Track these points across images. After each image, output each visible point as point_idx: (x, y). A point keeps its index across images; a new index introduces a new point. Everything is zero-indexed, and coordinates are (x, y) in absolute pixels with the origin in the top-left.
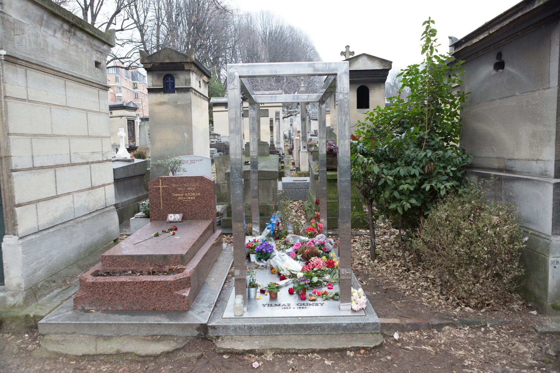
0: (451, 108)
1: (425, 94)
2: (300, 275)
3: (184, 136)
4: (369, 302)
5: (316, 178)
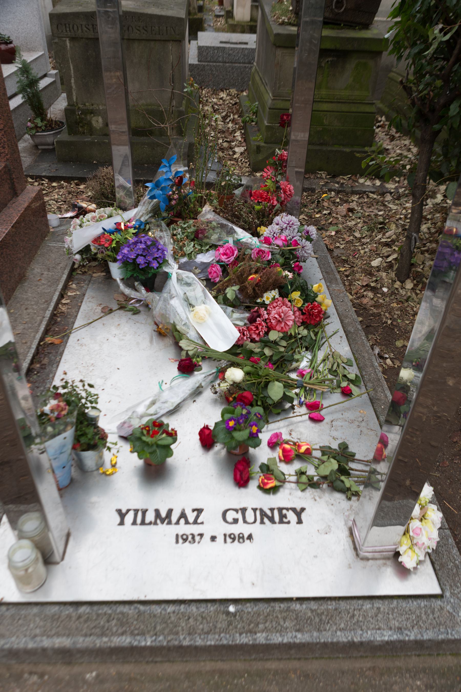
5: (287, 43)
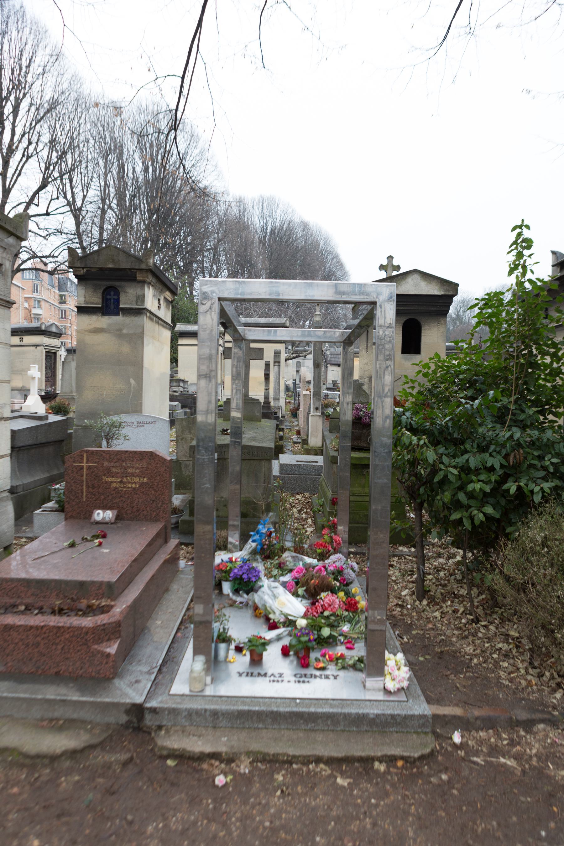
0: (552, 363)
1: (512, 338)
2: (302, 623)
3: (129, 383)
4: (413, 676)
5: (333, 461)
